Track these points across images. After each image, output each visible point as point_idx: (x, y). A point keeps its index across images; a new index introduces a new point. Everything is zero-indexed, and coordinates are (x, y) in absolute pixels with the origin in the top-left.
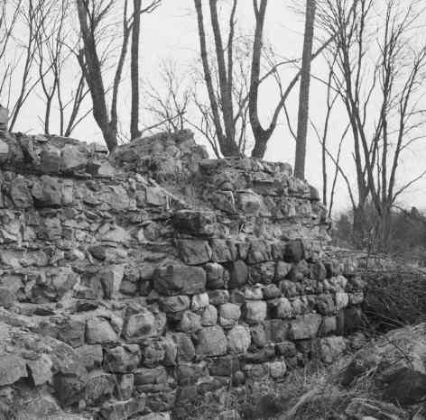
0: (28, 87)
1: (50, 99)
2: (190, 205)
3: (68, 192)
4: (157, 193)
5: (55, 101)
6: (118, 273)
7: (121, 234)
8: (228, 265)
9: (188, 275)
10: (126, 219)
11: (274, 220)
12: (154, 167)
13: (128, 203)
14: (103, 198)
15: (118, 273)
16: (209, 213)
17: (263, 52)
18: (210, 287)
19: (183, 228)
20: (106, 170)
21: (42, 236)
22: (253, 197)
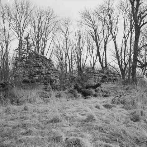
0: (88, 55)
1: (91, 56)
2: (106, 75)
3: (96, 74)
4: (103, 74)
5: (92, 57)
6: (100, 80)
7: (100, 77)
8: (109, 80)
9: (35, 61)
10: (100, 76)
11: (114, 76)
12: (104, 72)
13: (100, 75)
14: (99, 75)
15: (100, 80)
16: (107, 76)
17: (134, 42)
18: (107, 81)
19: (105, 77)
20: (99, 73)
21: (95, 77)
22: (111, 74)
